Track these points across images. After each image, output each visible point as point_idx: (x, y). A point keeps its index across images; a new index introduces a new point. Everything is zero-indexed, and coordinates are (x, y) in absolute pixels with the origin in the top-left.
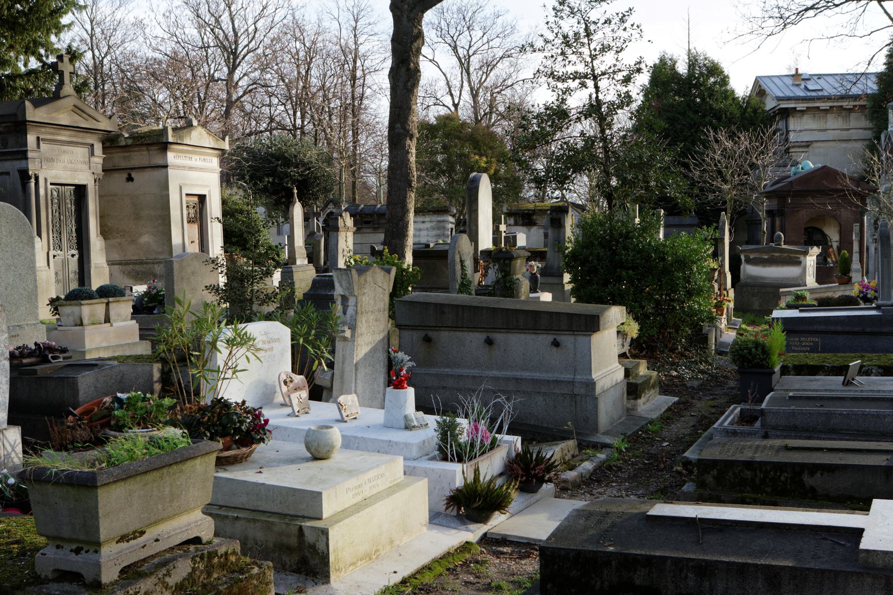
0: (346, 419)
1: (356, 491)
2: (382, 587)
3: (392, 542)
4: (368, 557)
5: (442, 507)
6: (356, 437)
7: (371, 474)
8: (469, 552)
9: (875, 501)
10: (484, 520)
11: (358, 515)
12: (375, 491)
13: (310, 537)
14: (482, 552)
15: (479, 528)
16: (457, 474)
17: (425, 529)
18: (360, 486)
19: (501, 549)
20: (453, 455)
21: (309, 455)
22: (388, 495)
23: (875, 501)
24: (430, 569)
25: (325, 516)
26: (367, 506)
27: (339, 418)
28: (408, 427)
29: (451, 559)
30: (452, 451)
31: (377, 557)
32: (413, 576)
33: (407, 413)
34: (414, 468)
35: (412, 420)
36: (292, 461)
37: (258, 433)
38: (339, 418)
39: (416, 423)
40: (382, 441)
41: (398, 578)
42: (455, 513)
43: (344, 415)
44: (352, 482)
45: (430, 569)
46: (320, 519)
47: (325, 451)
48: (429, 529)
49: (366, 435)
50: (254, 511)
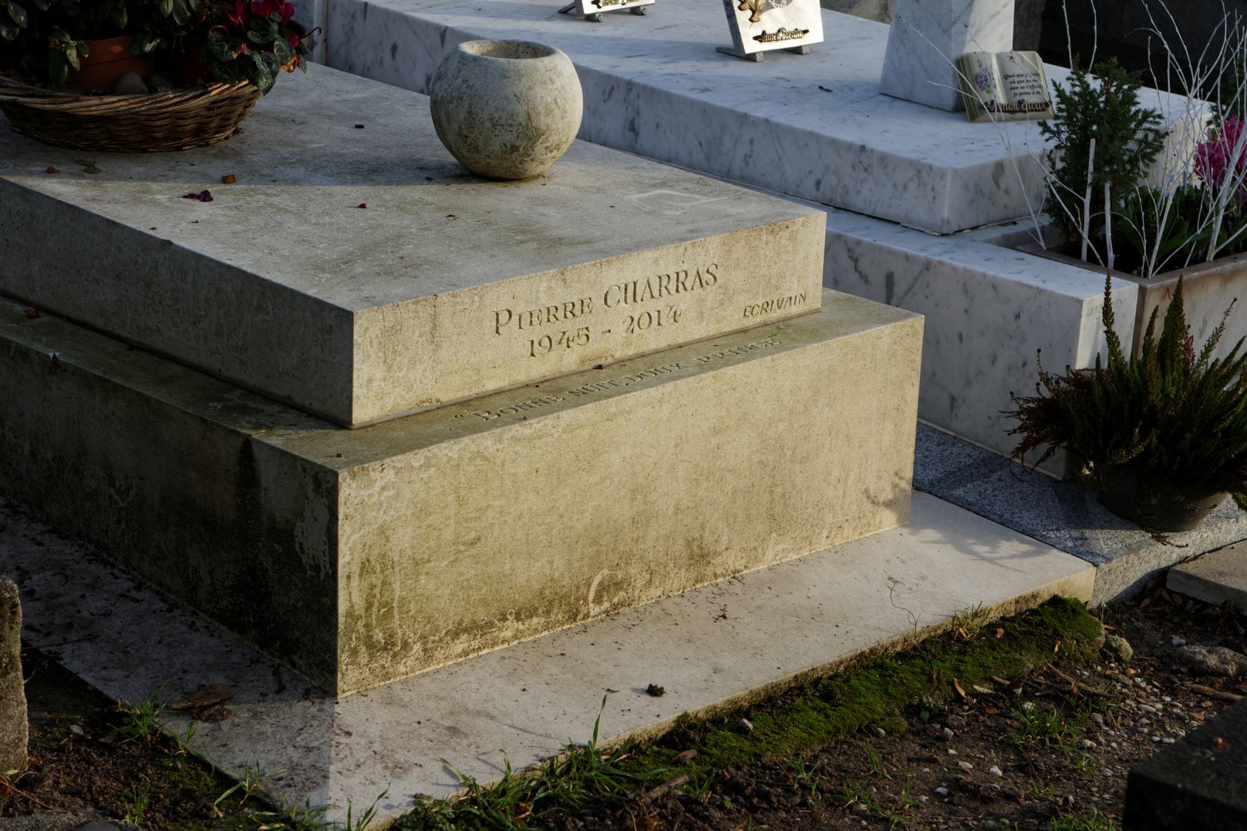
0: (750, 47)
1: (554, 330)
2: (554, 747)
3: (699, 556)
4: (561, 606)
5: (1005, 437)
6: (744, 118)
7: (640, 267)
8: (1045, 647)
9: (822, 40)
10: (1165, 517)
11: (517, 429)
12: (652, 339)
13: (276, 496)
14: (1109, 653)
15: (1130, 550)
16: (1093, 314)
17: (888, 521)
18: (571, 311)
19: (1200, 652)
20: (1100, 243)
21: (439, 153)
22: (706, 365)
23: (822, 40)
24: (827, 696)
25: (362, 412)
26: (582, 396)
27: (728, 41)
28: (965, 108)
29: (942, 668)
30: (1097, 223)
31: (612, 613)
32: (730, 719)
33: (969, 49)
34: (927, 266)
35: (983, 81)
36: (372, 171)
37: (235, 35)
38: (728, 41)
39: (1000, 98)
40: (835, 144)
41: (655, 719)
42: (1056, 468)
43: (748, 32)
44: (538, 289)
45: (827, 696)
46: (341, 421)
47: (496, 145)
48: (910, 521)
49: (780, 116)
50: (132, 346)
